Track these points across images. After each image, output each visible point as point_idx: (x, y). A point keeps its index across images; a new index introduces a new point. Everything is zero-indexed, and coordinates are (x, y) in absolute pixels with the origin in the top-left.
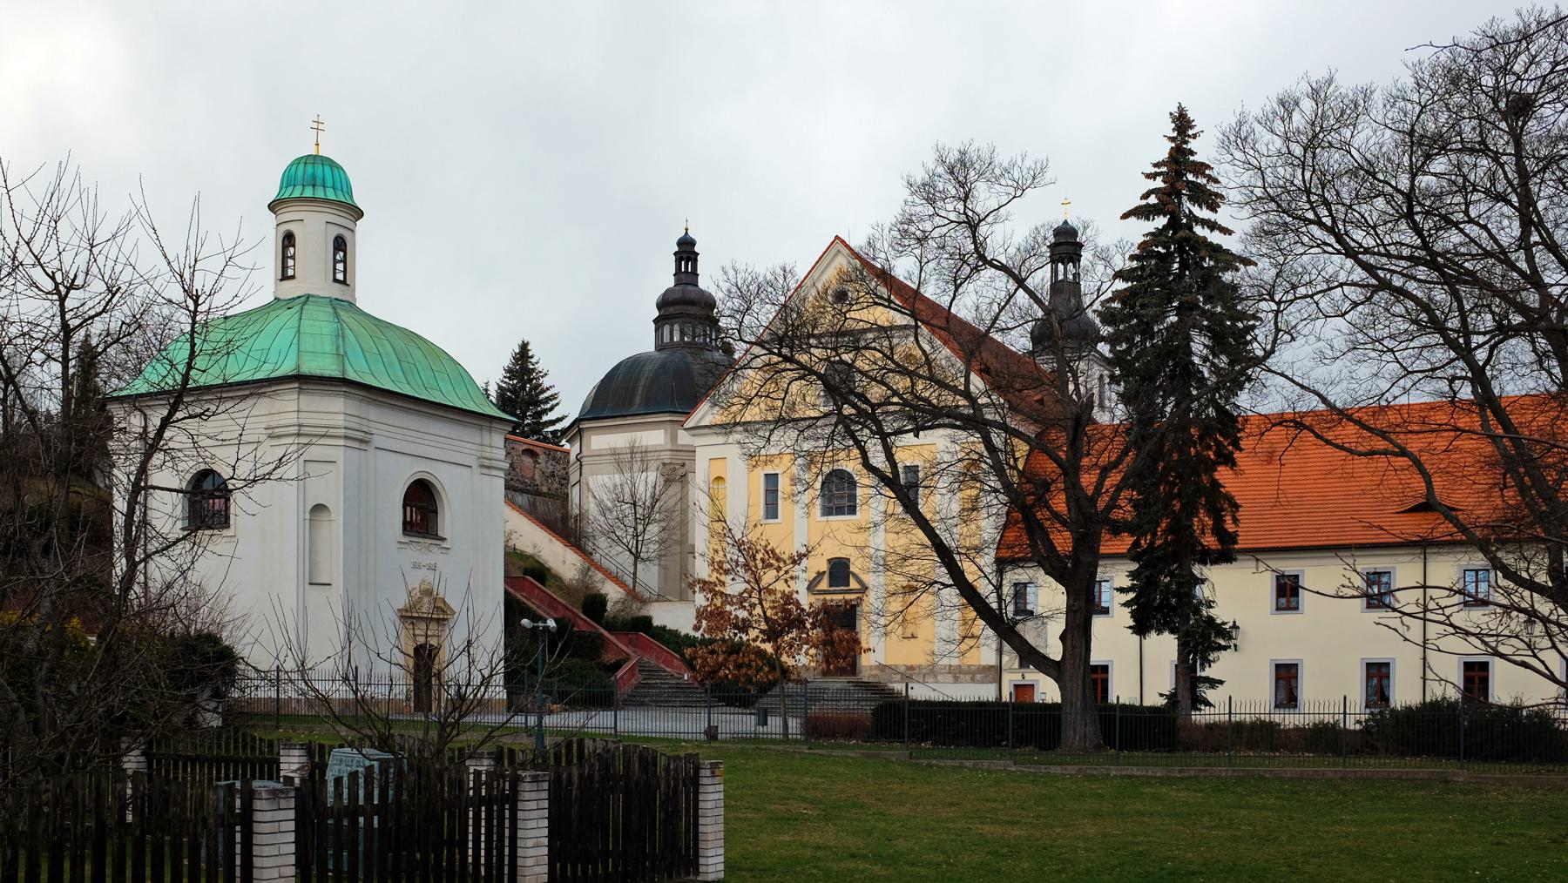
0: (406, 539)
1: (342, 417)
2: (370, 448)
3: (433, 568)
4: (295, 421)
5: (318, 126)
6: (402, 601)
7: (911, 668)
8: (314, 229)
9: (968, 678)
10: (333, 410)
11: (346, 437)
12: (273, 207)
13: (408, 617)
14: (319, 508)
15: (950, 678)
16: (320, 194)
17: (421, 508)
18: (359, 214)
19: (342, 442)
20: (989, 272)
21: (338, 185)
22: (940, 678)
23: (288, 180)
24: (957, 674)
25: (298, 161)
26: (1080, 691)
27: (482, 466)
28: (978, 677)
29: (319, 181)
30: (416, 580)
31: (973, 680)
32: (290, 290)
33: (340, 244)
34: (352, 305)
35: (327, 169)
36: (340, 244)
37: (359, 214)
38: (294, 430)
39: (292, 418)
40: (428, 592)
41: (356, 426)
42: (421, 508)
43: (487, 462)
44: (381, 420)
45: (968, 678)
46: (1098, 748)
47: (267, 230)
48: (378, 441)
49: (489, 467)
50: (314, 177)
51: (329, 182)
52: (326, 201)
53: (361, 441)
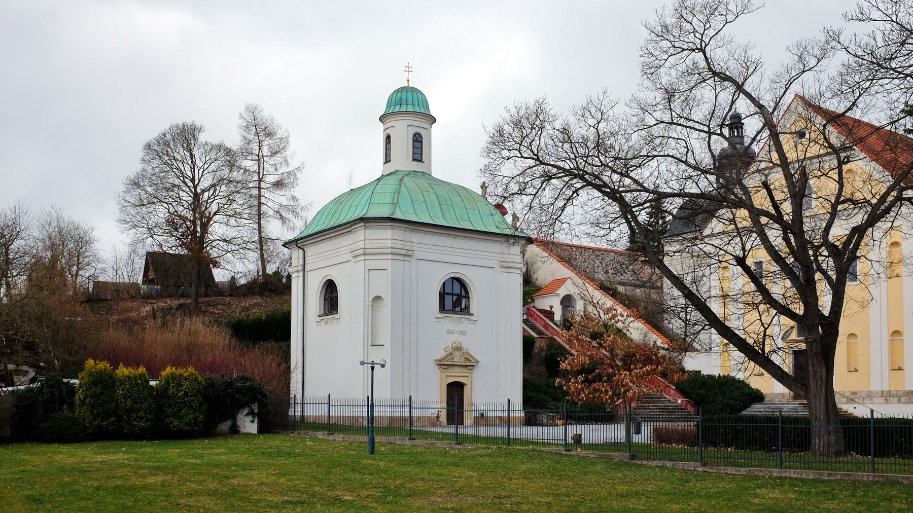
0: (442, 315)
1: (390, 241)
2: (413, 260)
3: (462, 333)
4: (390, 245)
5: (408, 69)
6: (441, 354)
7: (854, 393)
8: (402, 131)
9: (896, 399)
10: (385, 236)
11: (392, 254)
12: (382, 119)
13: (444, 365)
14: (378, 298)
15: (882, 400)
16: (404, 109)
17: (455, 298)
18: (433, 120)
19: (390, 257)
20: (701, 54)
21: (421, 104)
22: (875, 400)
23: (389, 105)
24: (887, 396)
25: (397, 91)
26: (823, 407)
27: (503, 267)
28: (903, 399)
29: (404, 102)
30: (450, 341)
31: (899, 401)
32: (391, 167)
33: (418, 140)
34: (426, 175)
35: (409, 94)
36: (418, 140)
37: (433, 120)
38: (361, 251)
39: (361, 244)
40: (459, 349)
41: (402, 247)
42: (455, 298)
43: (505, 264)
44: (419, 241)
45: (896, 399)
46: (838, 454)
47: (378, 133)
48: (418, 255)
49: (508, 268)
50: (401, 99)
51: (410, 101)
52: (407, 112)
53: (405, 255)
